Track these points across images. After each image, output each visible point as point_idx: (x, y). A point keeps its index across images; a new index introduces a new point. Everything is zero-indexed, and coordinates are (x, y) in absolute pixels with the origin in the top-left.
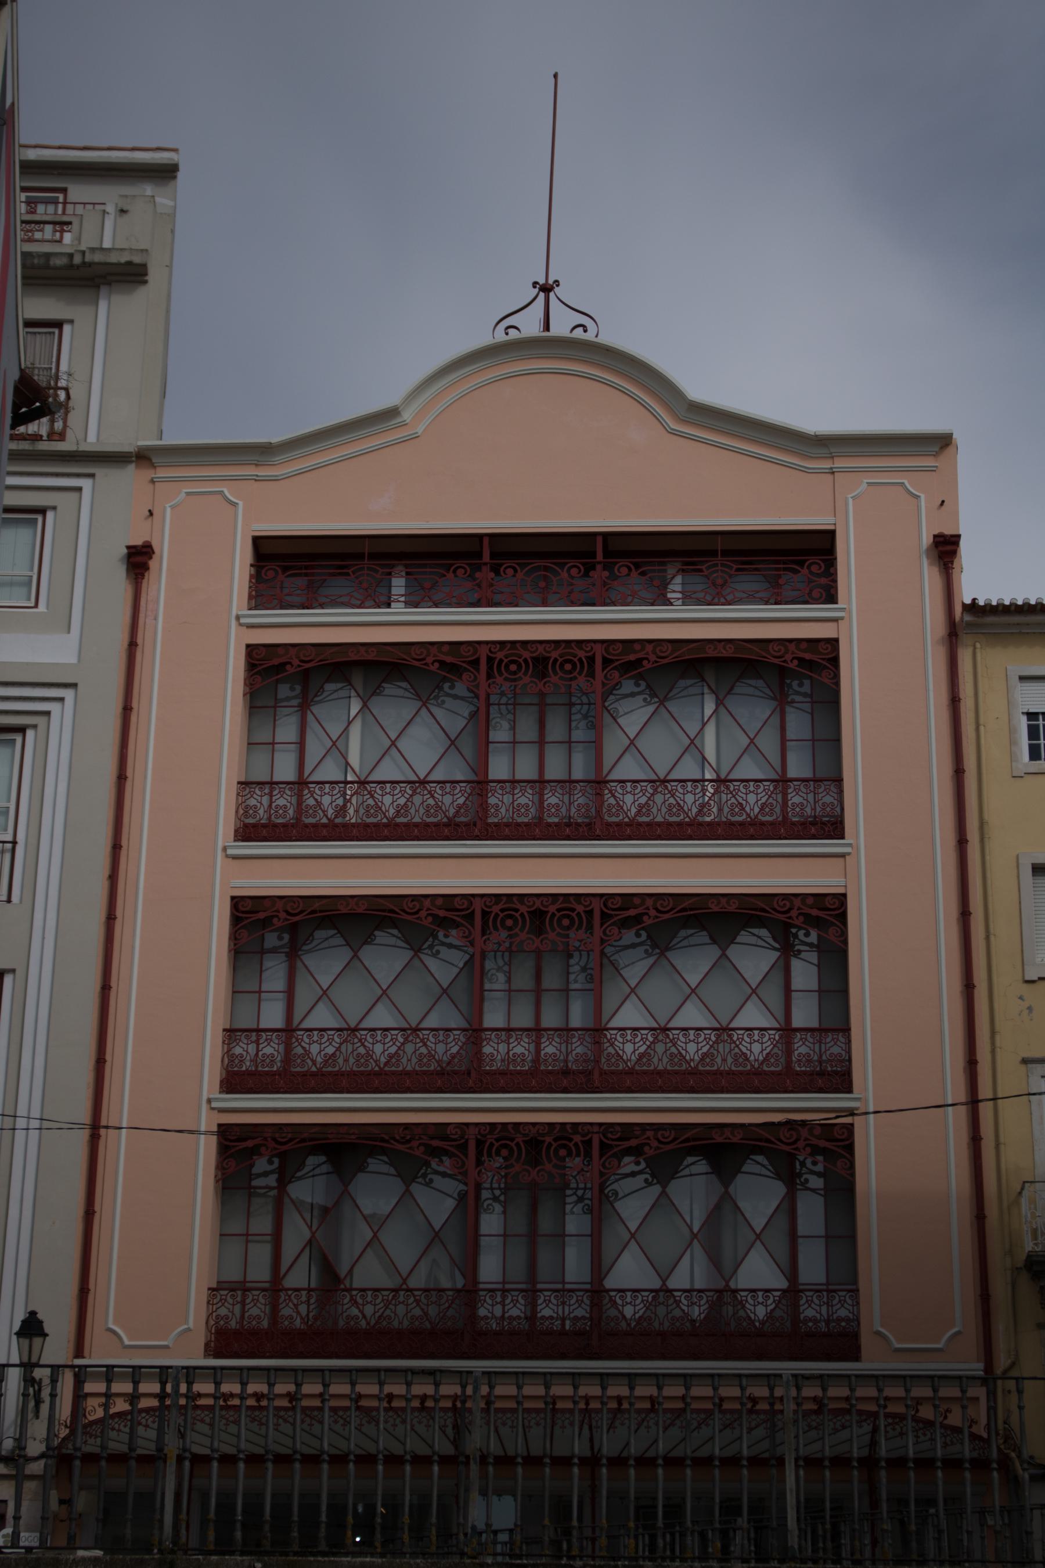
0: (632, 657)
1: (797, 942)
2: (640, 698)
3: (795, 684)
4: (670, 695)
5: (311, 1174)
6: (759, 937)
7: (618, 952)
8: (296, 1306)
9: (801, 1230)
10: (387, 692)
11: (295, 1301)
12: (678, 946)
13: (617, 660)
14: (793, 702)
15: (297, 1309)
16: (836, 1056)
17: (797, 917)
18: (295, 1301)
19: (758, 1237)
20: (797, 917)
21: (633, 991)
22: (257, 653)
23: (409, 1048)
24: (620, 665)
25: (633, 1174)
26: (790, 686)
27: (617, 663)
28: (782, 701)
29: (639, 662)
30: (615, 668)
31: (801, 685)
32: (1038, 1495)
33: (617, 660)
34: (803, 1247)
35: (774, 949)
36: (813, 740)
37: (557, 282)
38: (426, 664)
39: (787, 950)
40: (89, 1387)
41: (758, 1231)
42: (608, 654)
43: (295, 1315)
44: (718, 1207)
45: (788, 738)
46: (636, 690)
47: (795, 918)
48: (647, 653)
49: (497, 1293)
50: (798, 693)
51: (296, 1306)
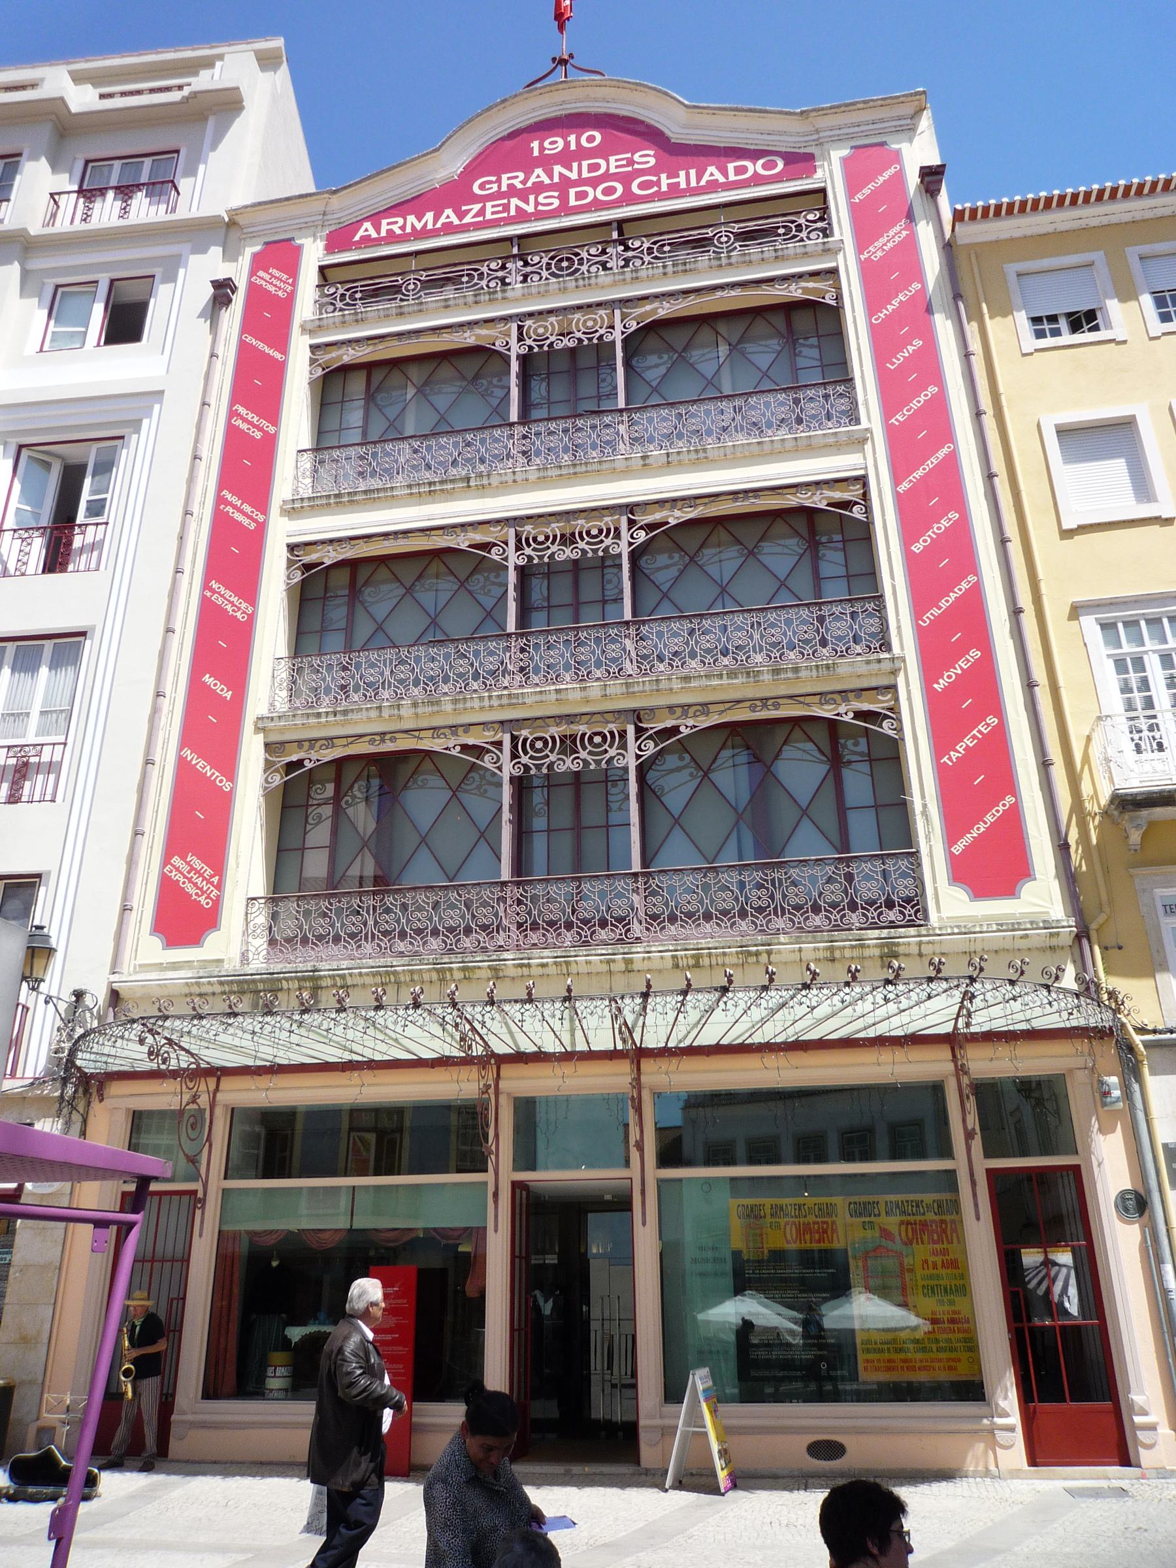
1: (846, 752)
2: (686, 772)
3: (850, 743)
4: (714, 766)
5: (416, 734)
6: (804, 751)
7: (663, 776)
9: (850, 800)
10: (445, 390)
14: (850, 762)
19: (805, 812)
21: (665, 595)
25: (679, 769)
26: (845, 746)
27: (651, 732)
28: (791, 338)
31: (856, 744)
32: (1169, 923)
34: (853, 818)
35: (822, 762)
36: (848, 576)
37: (554, 59)
39: (813, 546)
40: (530, 209)
41: (804, 805)
44: (761, 784)
45: (848, 806)
46: (681, 764)
50: (855, 753)
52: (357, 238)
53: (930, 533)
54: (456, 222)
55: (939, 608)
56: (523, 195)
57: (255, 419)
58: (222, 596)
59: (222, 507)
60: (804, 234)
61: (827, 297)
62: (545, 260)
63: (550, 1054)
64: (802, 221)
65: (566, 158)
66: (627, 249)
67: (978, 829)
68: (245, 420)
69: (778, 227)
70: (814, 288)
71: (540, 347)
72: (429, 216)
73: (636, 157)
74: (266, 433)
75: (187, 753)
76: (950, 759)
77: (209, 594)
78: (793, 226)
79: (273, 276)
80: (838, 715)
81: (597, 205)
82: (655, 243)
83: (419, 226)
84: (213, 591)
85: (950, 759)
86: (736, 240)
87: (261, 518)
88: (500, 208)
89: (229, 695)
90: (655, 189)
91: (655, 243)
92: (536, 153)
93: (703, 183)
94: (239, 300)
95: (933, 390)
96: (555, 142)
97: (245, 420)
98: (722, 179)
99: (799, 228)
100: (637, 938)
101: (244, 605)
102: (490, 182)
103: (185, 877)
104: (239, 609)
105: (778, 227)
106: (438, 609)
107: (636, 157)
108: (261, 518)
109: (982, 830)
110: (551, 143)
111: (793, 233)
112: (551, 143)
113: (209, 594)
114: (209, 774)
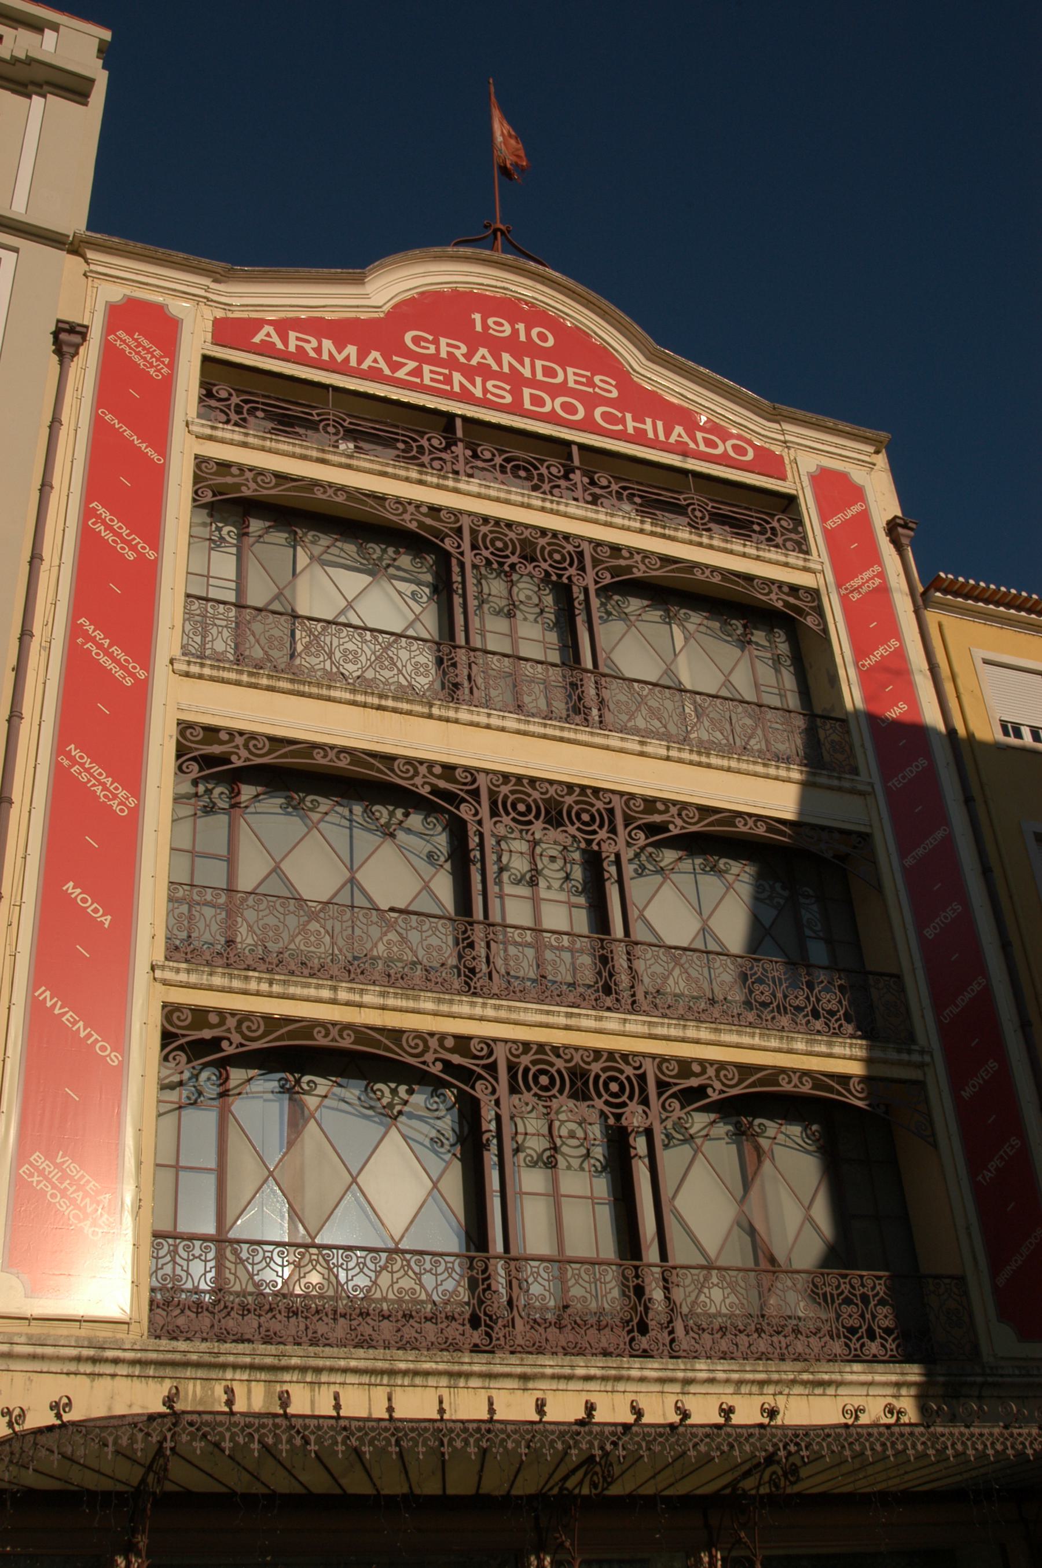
0: (207, 1034)
8: (418, 1276)
11: (417, 1269)
12: (410, 1142)
13: (184, 1036)
15: (420, 1280)
16: (407, 1293)
17: (434, 1063)
18: (417, 1269)
20: (434, 1063)
22: (178, 1018)
23: (385, 1279)
24: (187, 1043)
27: (183, 1041)
29: (215, 1044)
30: (181, 1048)
33: (184, 1036)
35: (807, 1152)
38: (424, 1063)
40: (478, 392)
42: (172, 1026)
43: (417, 1288)
47: (431, 1065)
48: (229, 1030)
49: (425, 1257)
51: (418, 1276)
52: (257, 340)
53: (938, 920)
54: (387, 371)
55: (957, 1006)
56: (470, 373)
57: (125, 532)
58: (87, 770)
59: (80, 640)
60: (426, 459)
61: (447, 540)
62: (235, 400)
63: (391, 1499)
64: (424, 443)
65: (511, 344)
66: (592, 483)
67: (1016, 1261)
68: (109, 528)
69: (397, 440)
70: (431, 526)
71: (560, 576)
72: (351, 350)
73: (597, 379)
74: (141, 556)
75: (45, 994)
76: (984, 1177)
77: (66, 763)
78: (414, 445)
79: (139, 345)
80: (424, 1063)
81: (551, 418)
82: (246, 402)
83: (340, 358)
84: (74, 761)
85: (984, 1177)
86: (711, 520)
87: (142, 674)
88: (441, 378)
89: (107, 920)
90: (620, 427)
91: (246, 402)
92: (479, 328)
93: (365, 366)
94: (90, 354)
95: (922, 762)
96: (501, 325)
97: (109, 528)
98: (280, 345)
99: (421, 449)
100: (645, 1351)
101: (122, 793)
102: (426, 340)
103: (54, 1187)
104: (115, 797)
105: (397, 440)
106: (348, 864)
107: (597, 379)
108: (142, 674)
109: (1020, 1262)
110: (495, 323)
111: (414, 453)
112: (495, 323)
113: (66, 763)
114: (82, 1034)
